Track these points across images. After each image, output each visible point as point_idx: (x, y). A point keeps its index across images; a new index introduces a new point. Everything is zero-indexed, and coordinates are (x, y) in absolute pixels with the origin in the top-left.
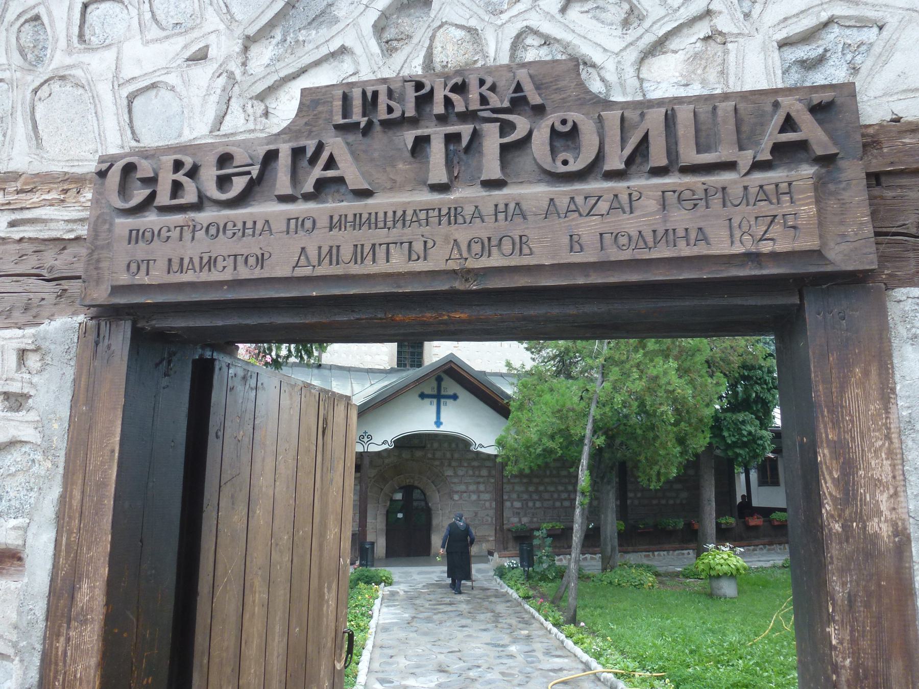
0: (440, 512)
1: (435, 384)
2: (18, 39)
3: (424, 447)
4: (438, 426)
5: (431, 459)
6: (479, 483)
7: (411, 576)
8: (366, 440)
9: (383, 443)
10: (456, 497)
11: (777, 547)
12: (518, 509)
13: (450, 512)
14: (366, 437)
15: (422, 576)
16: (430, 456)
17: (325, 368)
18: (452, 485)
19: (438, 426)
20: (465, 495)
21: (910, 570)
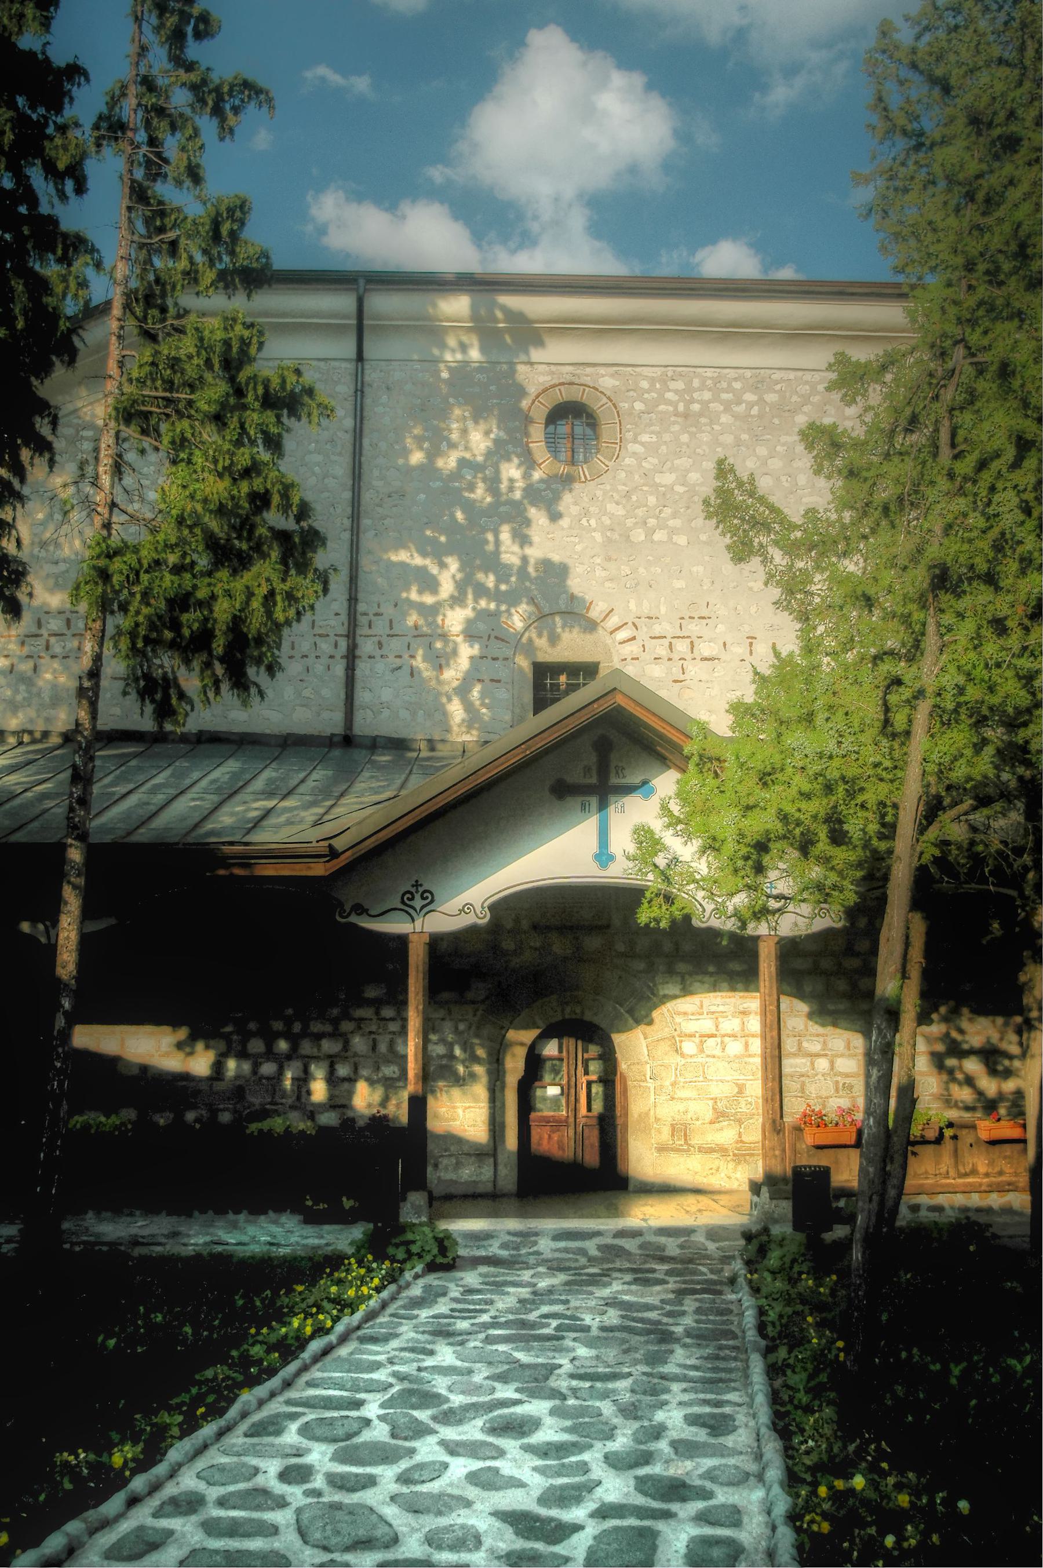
0: (651, 1084)
1: (591, 759)
2: (67, 287)
3: (608, 926)
4: (604, 865)
5: (623, 955)
6: (745, 1013)
7: (535, 1243)
8: (418, 903)
9: (462, 910)
10: (689, 1047)
11: (108, 839)
12: (847, 1075)
13: (674, 1084)
14: (418, 896)
15: (562, 1244)
16: (620, 947)
17: (360, 746)
18: (678, 1019)
19: (604, 865)
20: (711, 1042)
21: (805, 1174)
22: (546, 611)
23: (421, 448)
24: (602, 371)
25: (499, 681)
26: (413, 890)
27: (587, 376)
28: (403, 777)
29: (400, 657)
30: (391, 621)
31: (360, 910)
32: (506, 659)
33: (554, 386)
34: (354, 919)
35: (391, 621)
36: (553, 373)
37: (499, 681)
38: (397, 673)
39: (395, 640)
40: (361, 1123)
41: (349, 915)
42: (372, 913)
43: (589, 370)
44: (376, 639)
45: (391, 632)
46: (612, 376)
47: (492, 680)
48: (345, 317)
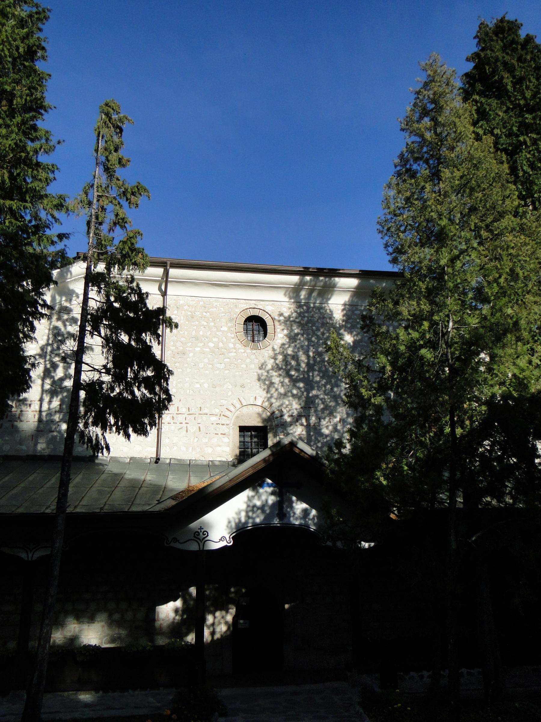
9: (221, 540)
22: (244, 404)
23: (405, 411)
24: (267, 303)
25: (225, 434)
26: (199, 531)
27: (260, 305)
28: (188, 478)
29: (182, 423)
30: (178, 407)
31: (176, 540)
32: (227, 425)
33: (247, 309)
34: (173, 544)
35: (178, 407)
36: (247, 303)
37: (225, 434)
38: (181, 430)
39: (180, 415)
40: (103, 616)
41: (171, 543)
42: (180, 541)
43: (262, 303)
44: (171, 415)
45: (178, 413)
46: (271, 305)
47: (221, 434)
48: (180, 282)
